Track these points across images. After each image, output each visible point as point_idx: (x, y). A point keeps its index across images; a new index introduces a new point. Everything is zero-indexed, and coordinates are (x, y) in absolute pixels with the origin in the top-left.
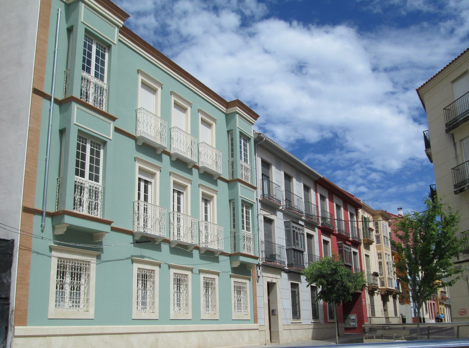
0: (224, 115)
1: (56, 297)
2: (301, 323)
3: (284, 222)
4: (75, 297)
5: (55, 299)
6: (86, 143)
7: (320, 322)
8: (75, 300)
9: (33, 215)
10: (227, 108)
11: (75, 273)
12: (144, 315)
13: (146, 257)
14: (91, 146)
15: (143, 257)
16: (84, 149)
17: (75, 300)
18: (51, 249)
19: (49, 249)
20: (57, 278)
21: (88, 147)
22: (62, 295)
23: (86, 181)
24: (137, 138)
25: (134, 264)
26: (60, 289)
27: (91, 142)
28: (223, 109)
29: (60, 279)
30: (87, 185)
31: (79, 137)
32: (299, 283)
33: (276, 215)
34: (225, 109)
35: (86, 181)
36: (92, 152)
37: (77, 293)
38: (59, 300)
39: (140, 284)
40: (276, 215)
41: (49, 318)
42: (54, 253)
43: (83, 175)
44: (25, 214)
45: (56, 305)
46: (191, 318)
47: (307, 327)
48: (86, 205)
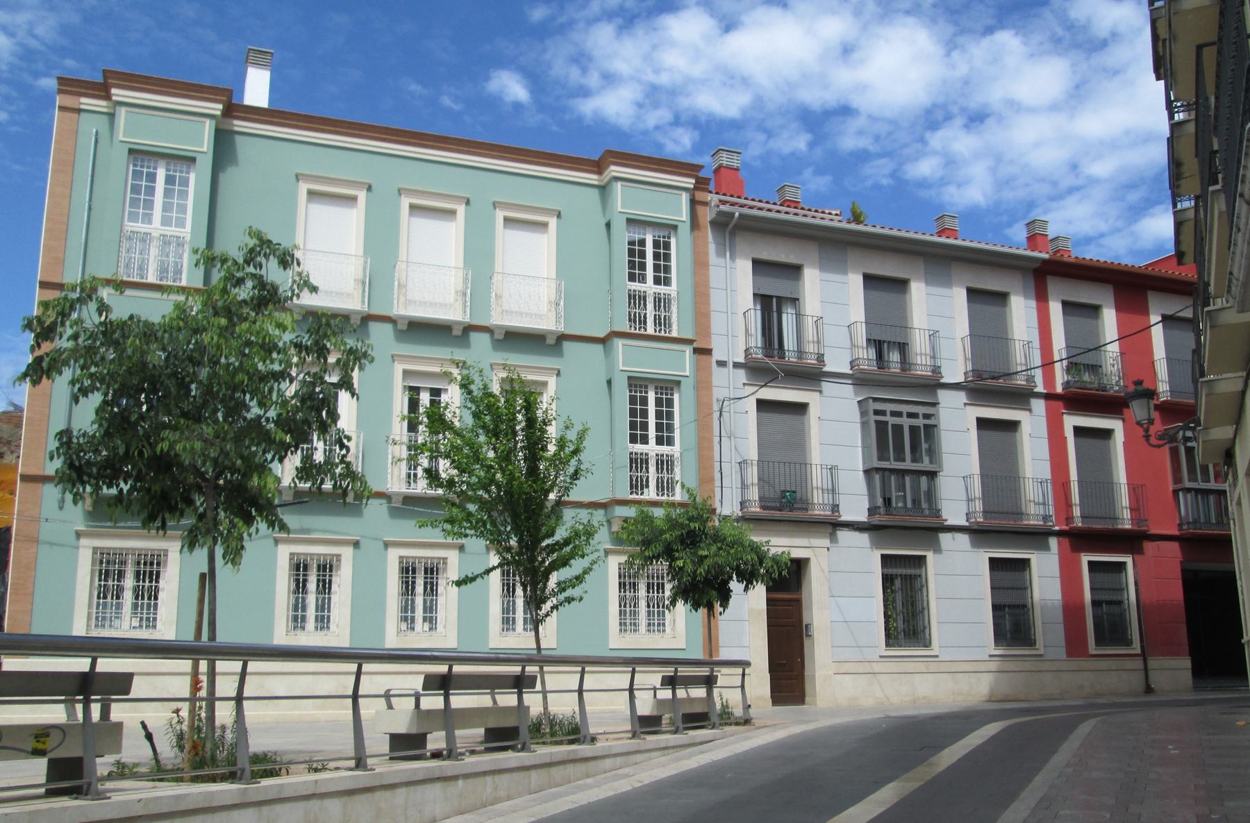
0: (596, 192)
1: (620, 619)
2: (937, 656)
3: (859, 402)
4: (145, 611)
5: (618, 621)
6: (646, 392)
7: (1041, 655)
8: (145, 616)
9: (41, 485)
10: (600, 172)
11: (145, 572)
12: (309, 638)
13: (315, 530)
14: (656, 393)
15: (308, 531)
16: (644, 401)
17: (145, 616)
18: (79, 535)
19: (75, 535)
20: (620, 592)
21: (651, 396)
22: (635, 615)
23: (652, 448)
24: (394, 318)
25: (390, 550)
26: (112, 598)
27: (656, 388)
28: (393, 149)
29: (114, 581)
30: (652, 454)
31: (630, 385)
32: (930, 555)
33: (1030, 410)
34: (595, 177)
35: (652, 448)
36: (659, 402)
37: (149, 605)
38: (111, 617)
39: (420, 585)
40: (1030, 410)
41: (611, 647)
42: (84, 542)
43: (645, 440)
44: (24, 484)
45: (621, 630)
46: (684, 647)
47: (982, 667)
48: (652, 484)
